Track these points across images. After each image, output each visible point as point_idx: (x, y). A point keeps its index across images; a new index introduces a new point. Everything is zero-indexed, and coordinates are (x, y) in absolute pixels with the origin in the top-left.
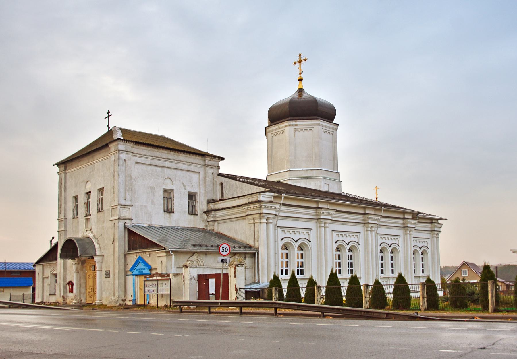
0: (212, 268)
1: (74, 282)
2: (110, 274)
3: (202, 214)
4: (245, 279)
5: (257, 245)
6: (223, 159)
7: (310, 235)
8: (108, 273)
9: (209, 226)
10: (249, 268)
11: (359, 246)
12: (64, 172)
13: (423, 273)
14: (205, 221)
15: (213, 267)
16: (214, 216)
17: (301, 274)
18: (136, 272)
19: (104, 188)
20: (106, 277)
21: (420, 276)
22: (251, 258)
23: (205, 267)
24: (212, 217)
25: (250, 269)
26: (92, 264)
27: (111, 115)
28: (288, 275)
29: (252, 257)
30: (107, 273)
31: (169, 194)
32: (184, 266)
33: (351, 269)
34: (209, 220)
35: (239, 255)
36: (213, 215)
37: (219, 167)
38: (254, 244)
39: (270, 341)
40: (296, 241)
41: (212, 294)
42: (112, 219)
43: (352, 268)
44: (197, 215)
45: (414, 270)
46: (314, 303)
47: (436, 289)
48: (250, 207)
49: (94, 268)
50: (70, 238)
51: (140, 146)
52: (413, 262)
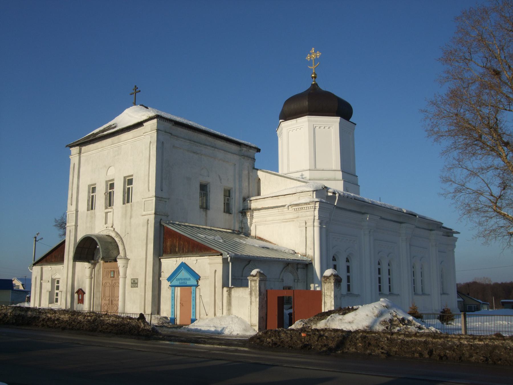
1: (87, 291)
2: (138, 284)
6: (258, 150)
8: (136, 282)
12: (78, 155)
18: (175, 282)
19: (133, 175)
20: (132, 287)
26: (111, 269)
27: (140, 91)
30: (134, 281)
31: (204, 188)
37: (255, 159)
39: (117, 320)
42: (144, 213)
45: (414, 287)
48: (302, 208)
49: (113, 274)
50: (90, 236)
51: (179, 127)
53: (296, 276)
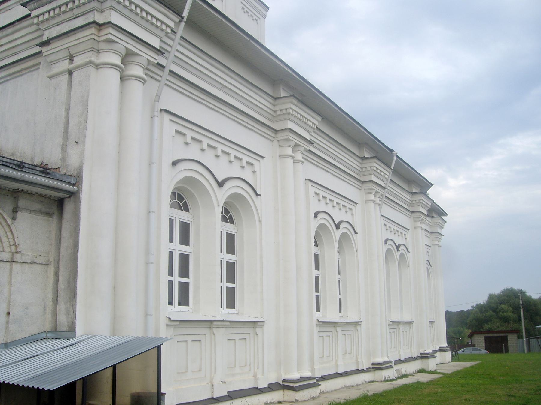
4: (8, 313)
5: (73, 162)
7: (258, 173)
11: (257, 200)
13: (231, 304)
17: (180, 304)
21: (211, 322)
22: (45, 218)
28: (227, 308)
29: (49, 215)
32: (50, 265)
33: (181, 284)
38: (63, 159)
40: (220, 181)
43: (231, 285)
45: (318, 298)
52: (338, 277)
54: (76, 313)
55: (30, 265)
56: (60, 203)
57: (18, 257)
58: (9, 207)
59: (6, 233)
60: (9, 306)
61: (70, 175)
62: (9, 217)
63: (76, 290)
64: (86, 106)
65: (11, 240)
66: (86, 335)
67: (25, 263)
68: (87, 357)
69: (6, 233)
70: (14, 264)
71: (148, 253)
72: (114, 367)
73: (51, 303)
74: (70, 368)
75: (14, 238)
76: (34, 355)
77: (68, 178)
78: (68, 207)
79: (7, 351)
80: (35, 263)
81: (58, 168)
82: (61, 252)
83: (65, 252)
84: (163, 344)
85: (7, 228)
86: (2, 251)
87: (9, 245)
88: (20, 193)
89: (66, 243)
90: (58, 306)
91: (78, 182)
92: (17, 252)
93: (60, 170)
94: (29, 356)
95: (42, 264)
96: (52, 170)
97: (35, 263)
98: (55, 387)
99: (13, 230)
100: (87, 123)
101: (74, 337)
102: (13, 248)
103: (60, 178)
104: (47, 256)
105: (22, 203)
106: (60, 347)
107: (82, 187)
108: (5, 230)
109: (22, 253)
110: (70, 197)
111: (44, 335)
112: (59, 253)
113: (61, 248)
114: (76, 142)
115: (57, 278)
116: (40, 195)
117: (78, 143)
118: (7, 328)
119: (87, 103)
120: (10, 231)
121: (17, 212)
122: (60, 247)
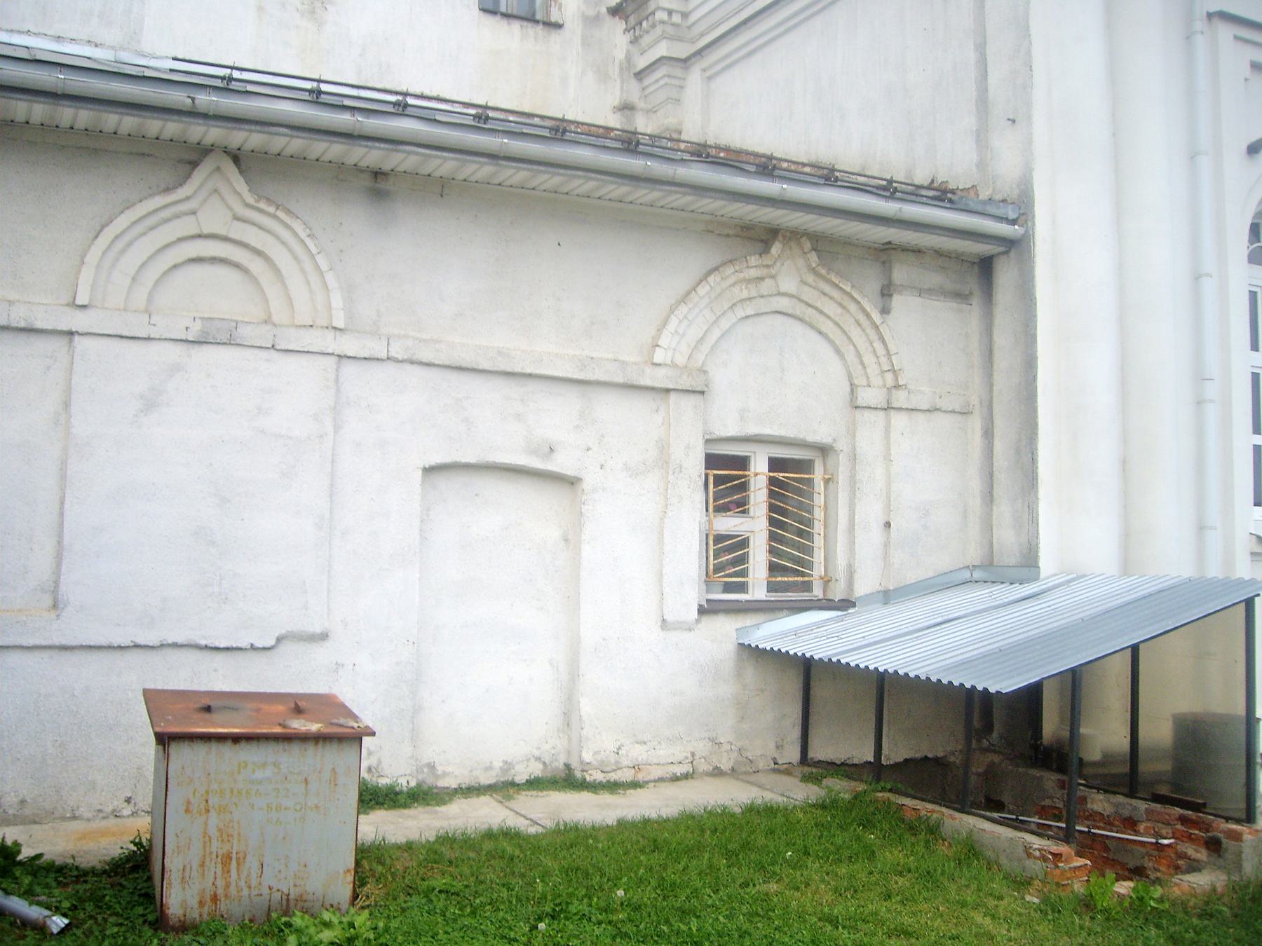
0: (460, 369)
3: (591, 21)
4: (888, 525)
5: (1006, 166)
9: (651, 111)
10: (934, 410)
14: (614, 71)
15: (467, 359)
16: (676, 19)
23: (349, 345)
24: (659, 30)
25: (939, 418)
29: (961, 297)
34: (642, 63)
35: (813, 257)
36: (670, 13)
41: (249, 647)
44: (558, 26)
46: (715, 476)
47: (345, 718)
53: (869, 359)
54: (1038, 524)
55: (928, 414)
56: (985, 267)
57: (900, 399)
58: (874, 285)
59: (871, 344)
60: (888, 508)
61: (1004, 201)
62: (876, 307)
63: (1037, 468)
64: (1024, 32)
65: (883, 360)
66: (1063, 573)
67: (916, 410)
68: (1075, 622)
69: (871, 344)
70: (892, 413)
71: (1200, 378)
72: (1135, 649)
73: (978, 501)
74: (1038, 647)
75: (889, 354)
76: (950, 617)
77: (998, 208)
78: (1005, 276)
79: (891, 609)
80: (938, 409)
81: (973, 186)
82: (995, 383)
83: (1005, 380)
84: (1258, 595)
85: (872, 334)
86: (865, 384)
87: (879, 372)
88: (893, 252)
89: (1005, 359)
90: (994, 508)
91: (1023, 214)
92: (897, 387)
93: (977, 190)
94: (940, 620)
95: (953, 412)
96: (959, 193)
97: (938, 409)
98: (1012, 685)
99: (887, 338)
100: (1031, 70)
101: (1036, 578)
102: (889, 377)
103: (979, 208)
104: (963, 392)
105: (900, 274)
106: (1006, 600)
107: (1034, 224)
108: (867, 336)
109: (909, 387)
110: (1006, 253)
111: (966, 575)
112: (991, 386)
113: (995, 374)
114: (1009, 119)
115: (989, 443)
116: (939, 253)
117: (1014, 121)
118: (886, 556)
119: (1028, 22)
120: (880, 339)
121: (891, 295)
122: (992, 371)
